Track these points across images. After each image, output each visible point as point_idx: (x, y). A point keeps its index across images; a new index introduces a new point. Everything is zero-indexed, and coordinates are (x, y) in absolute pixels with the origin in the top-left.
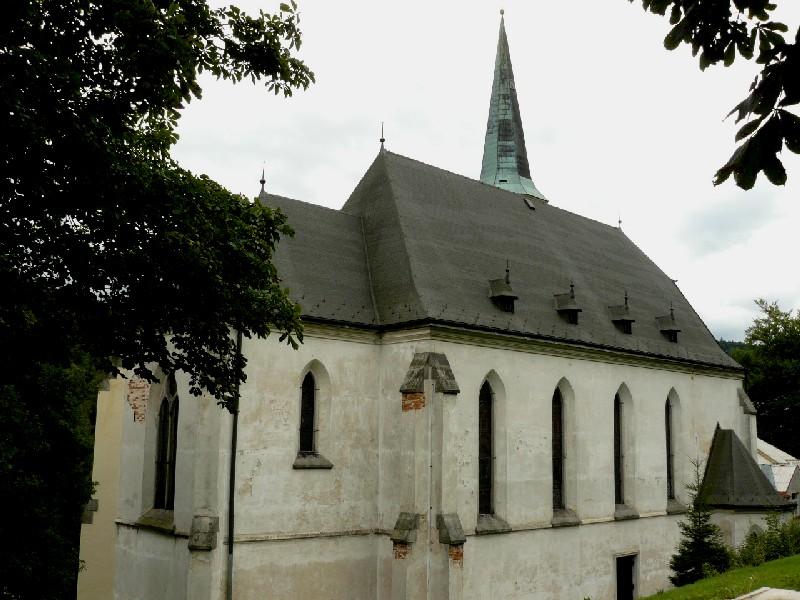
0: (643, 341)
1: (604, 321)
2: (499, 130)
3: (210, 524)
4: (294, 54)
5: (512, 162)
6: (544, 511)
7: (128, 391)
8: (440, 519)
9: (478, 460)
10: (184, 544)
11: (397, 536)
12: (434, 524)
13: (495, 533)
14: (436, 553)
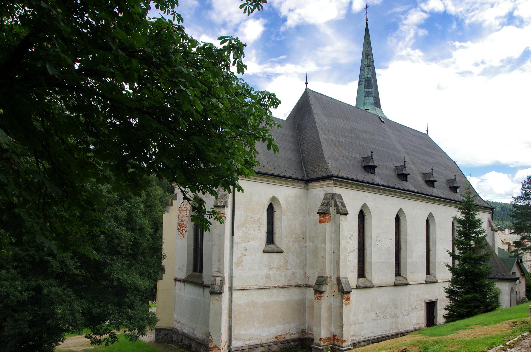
0: (440, 192)
1: (420, 180)
2: (365, 83)
3: (221, 280)
4: (237, 183)
5: (372, 100)
6: (390, 277)
7: (179, 213)
8: (338, 279)
9: (357, 250)
10: (207, 291)
11: (316, 287)
12: (335, 282)
13: (366, 287)
14: (336, 298)
